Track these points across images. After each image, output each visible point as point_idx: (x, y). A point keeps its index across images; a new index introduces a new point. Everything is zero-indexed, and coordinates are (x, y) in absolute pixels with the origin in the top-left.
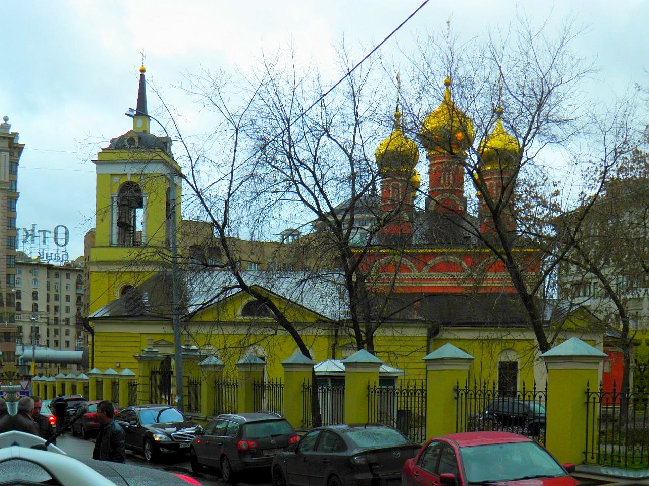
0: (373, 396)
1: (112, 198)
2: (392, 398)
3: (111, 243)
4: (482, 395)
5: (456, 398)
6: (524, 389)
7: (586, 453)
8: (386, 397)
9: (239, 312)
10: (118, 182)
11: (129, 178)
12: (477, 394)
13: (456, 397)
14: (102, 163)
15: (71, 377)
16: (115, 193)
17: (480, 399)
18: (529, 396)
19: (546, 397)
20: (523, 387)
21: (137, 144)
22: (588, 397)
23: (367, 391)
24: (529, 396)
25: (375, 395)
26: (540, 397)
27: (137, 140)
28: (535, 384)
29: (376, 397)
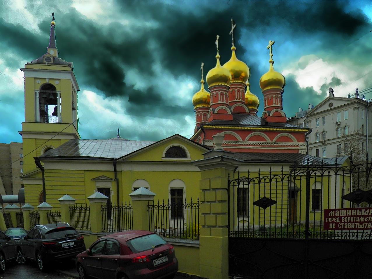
0: (104, 211)
1: (36, 93)
2: (152, 211)
3: (36, 120)
4: (162, 207)
5: (147, 210)
6: (192, 202)
7: (103, 228)
8: (152, 211)
9: (164, 155)
10: (40, 83)
11: (47, 81)
12: (131, 208)
13: (148, 209)
14: (28, 71)
15: (28, 207)
16: (38, 89)
17: (124, 210)
18: (195, 206)
19: (198, 207)
20: (163, 202)
21: (52, 62)
22: (149, 208)
23: (69, 209)
24: (195, 206)
25: (130, 210)
26: (166, 208)
27: (52, 59)
28: (163, 202)
29: (116, 211)
